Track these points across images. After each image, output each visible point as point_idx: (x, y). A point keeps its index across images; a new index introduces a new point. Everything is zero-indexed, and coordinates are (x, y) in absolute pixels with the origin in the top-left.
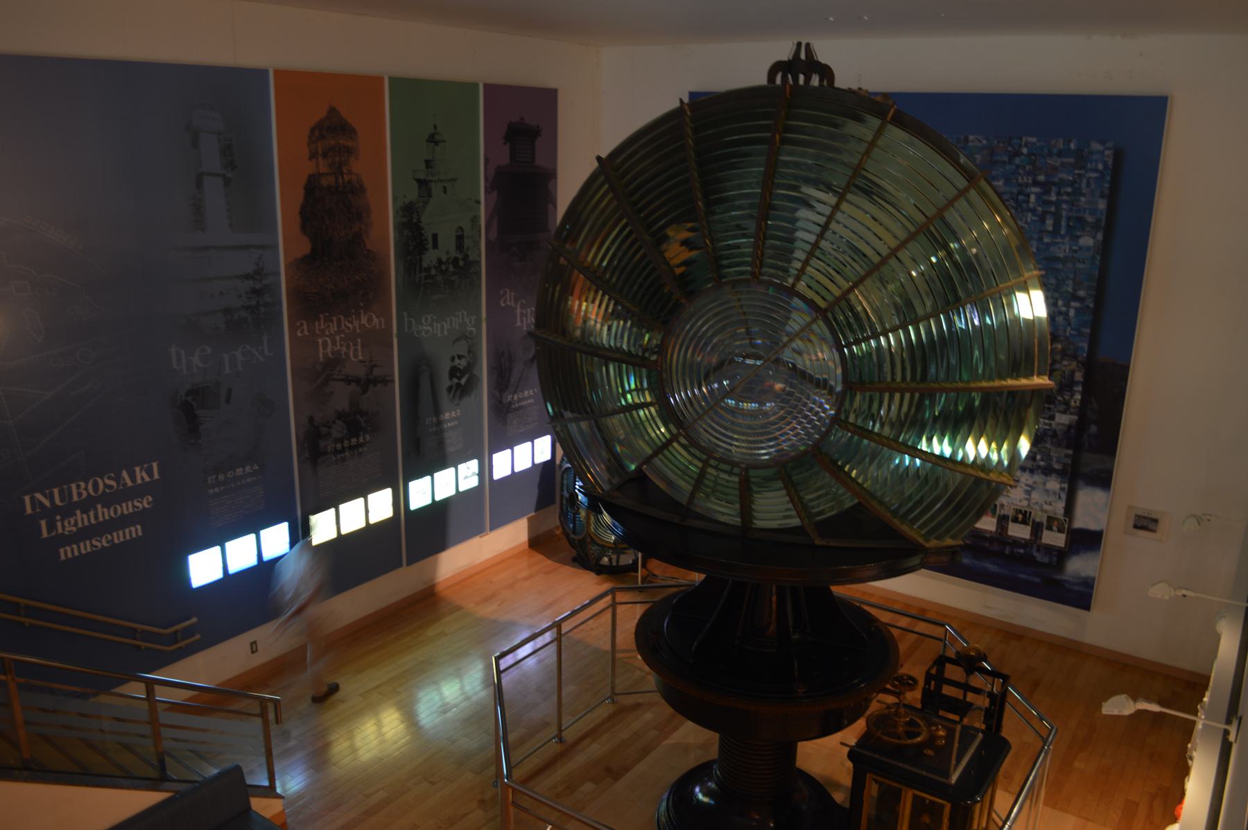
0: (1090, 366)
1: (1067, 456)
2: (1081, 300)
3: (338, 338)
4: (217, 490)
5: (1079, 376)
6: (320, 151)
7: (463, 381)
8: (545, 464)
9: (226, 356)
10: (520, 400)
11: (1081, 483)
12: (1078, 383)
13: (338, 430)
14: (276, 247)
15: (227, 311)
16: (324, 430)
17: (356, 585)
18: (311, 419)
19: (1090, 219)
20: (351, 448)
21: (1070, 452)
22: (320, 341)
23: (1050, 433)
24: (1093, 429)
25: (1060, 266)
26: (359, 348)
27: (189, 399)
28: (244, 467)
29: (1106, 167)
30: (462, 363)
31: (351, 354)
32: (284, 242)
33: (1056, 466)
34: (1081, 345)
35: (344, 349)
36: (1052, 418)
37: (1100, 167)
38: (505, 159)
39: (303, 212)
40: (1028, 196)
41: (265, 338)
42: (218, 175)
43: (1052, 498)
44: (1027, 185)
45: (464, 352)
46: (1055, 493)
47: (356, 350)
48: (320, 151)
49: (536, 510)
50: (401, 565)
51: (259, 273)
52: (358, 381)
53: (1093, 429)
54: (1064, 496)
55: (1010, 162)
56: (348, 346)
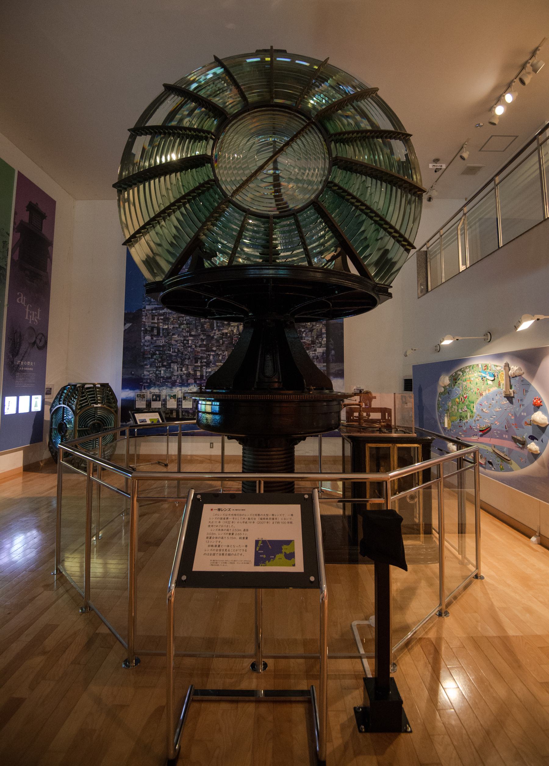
1: (324, 366)
5: (324, 331)
10: (25, 366)
17: (259, 504)
21: (325, 364)
23: (315, 357)
24: (333, 352)
36: (315, 350)
38: (26, 219)
40: (188, 341)
44: (187, 337)
49: (31, 443)
53: (333, 352)
55: (152, 358)
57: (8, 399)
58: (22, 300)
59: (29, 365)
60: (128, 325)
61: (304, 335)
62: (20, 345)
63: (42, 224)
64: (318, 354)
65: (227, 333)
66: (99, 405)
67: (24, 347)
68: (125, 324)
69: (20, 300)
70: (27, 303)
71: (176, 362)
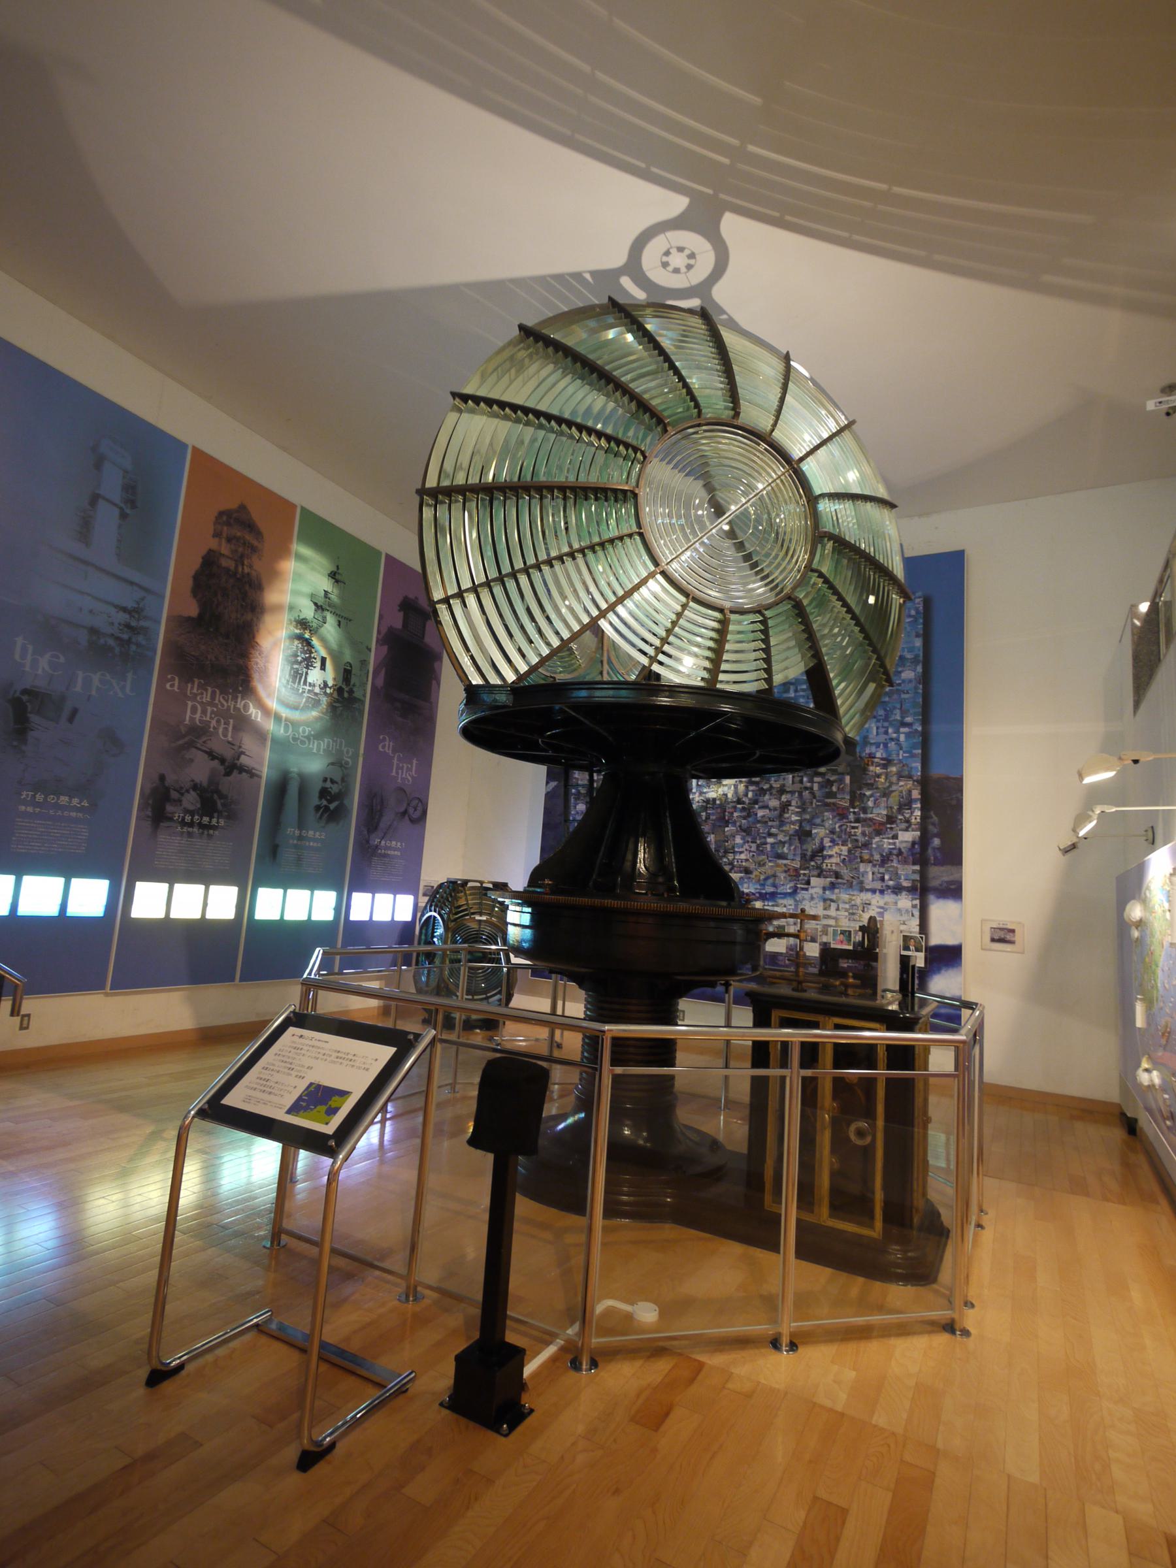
0: (925, 783)
1: (914, 872)
2: (909, 725)
3: (209, 709)
4: (30, 809)
5: (916, 794)
6: (224, 535)
7: (332, 806)
8: (406, 923)
9: (80, 675)
10: (387, 848)
11: (931, 897)
12: (916, 800)
13: (191, 800)
14: (163, 597)
15: (93, 631)
16: (174, 795)
18: (162, 778)
19: (909, 656)
20: (202, 826)
21: (917, 868)
22: (190, 704)
23: (895, 852)
25: (887, 699)
26: (230, 729)
27: (25, 698)
28: (71, 798)
29: (917, 612)
30: (335, 789)
31: (221, 731)
32: (171, 598)
33: (906, 884)
34: (914, 765)
35: (214, 723)
36: (895, 837)
37: (913, 612)
38: (398, 624)
39: (196, 578)
41: (130, 676)
42: (115, 505)
43: (905, 917)
45: (337, 778)
46: (907, 911)
47: (226, 729)
48: (224, 535)
50: (233, 980)
51: (135, 612)
52: (222, 761)
54: (917, 913)
56: (218, 722)
57: (356, 896)
58: (387, 746)
59: (394, 846)
60: (553, 784)
61: (870, 804)
62: (381, 816)
63: (424, 627)
64: (903, 846)
65: (714, 800)
66: (484, 918)
67: (385, 821)
68: (547, 783)
69: (384, 747)
70: (394, 751)
71: (870, 862)
